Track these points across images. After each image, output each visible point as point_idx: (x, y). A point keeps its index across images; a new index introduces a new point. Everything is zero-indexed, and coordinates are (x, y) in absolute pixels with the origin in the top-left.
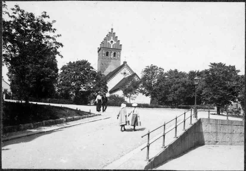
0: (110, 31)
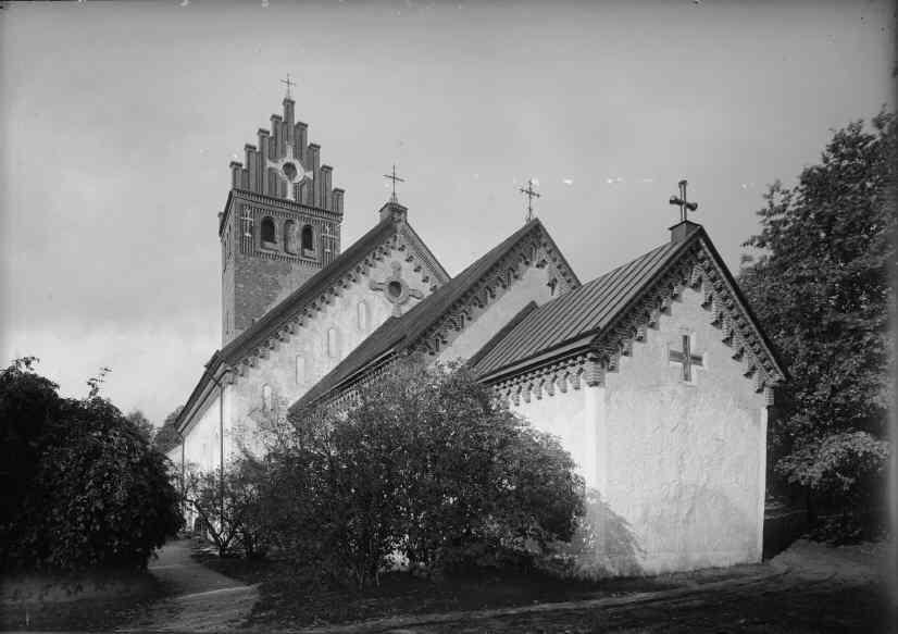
0: (281, 112)
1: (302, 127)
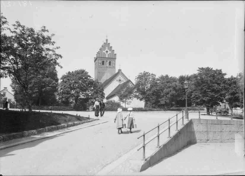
1: (109, 44)
